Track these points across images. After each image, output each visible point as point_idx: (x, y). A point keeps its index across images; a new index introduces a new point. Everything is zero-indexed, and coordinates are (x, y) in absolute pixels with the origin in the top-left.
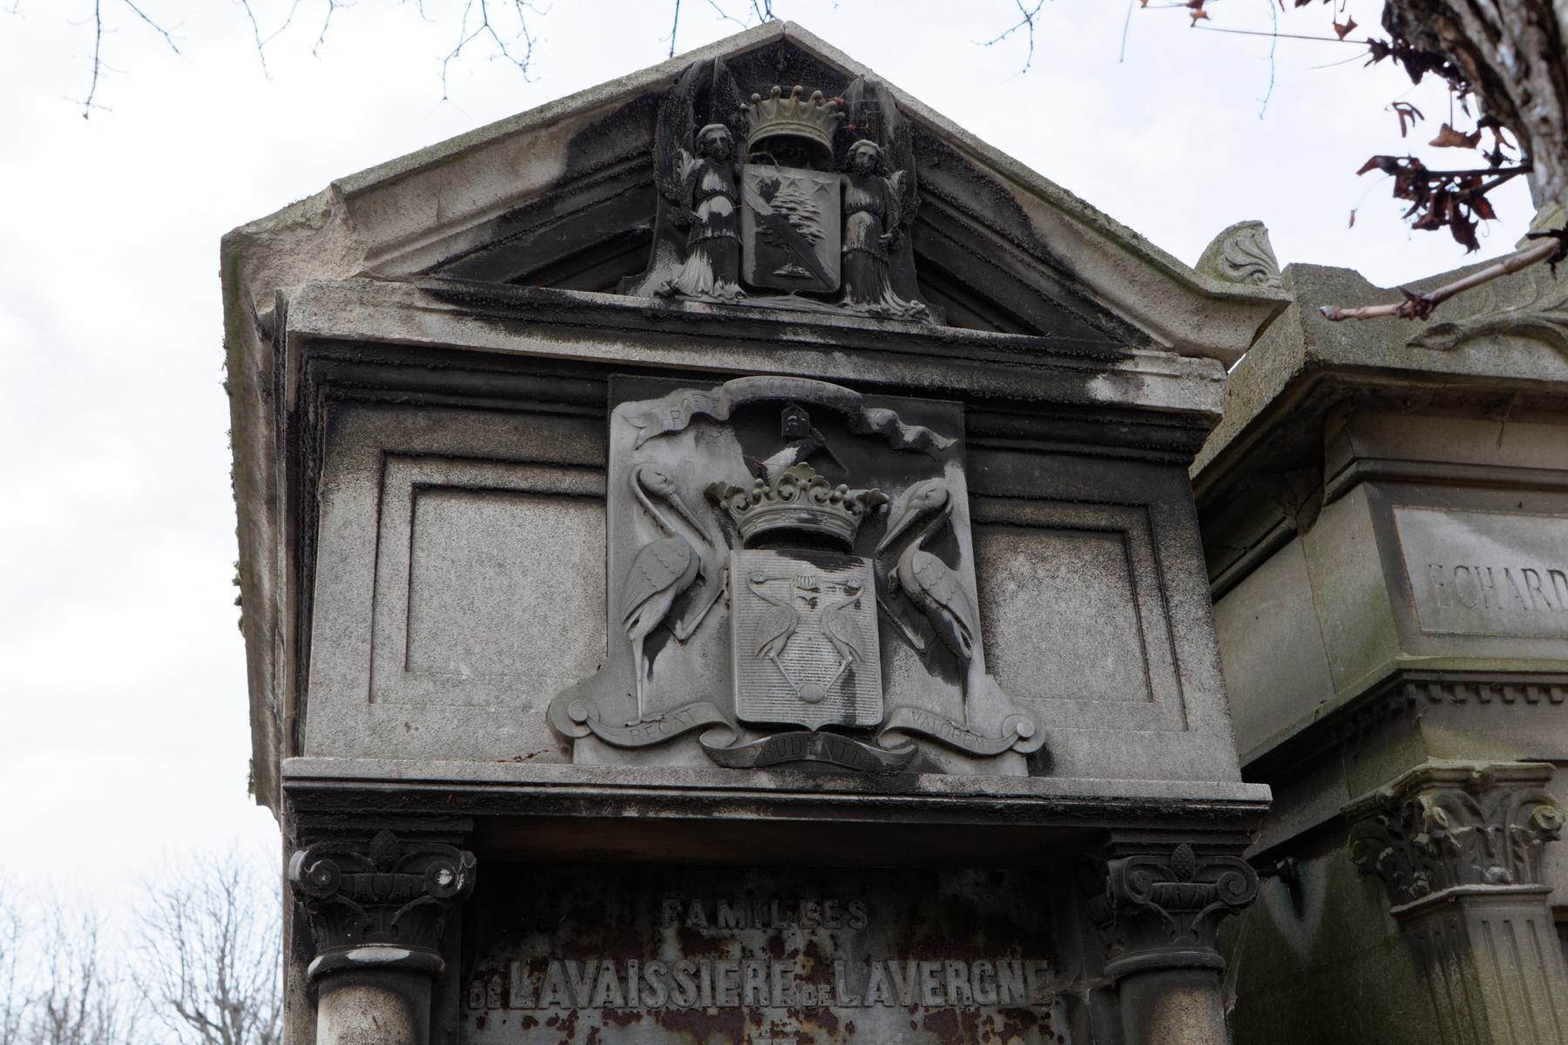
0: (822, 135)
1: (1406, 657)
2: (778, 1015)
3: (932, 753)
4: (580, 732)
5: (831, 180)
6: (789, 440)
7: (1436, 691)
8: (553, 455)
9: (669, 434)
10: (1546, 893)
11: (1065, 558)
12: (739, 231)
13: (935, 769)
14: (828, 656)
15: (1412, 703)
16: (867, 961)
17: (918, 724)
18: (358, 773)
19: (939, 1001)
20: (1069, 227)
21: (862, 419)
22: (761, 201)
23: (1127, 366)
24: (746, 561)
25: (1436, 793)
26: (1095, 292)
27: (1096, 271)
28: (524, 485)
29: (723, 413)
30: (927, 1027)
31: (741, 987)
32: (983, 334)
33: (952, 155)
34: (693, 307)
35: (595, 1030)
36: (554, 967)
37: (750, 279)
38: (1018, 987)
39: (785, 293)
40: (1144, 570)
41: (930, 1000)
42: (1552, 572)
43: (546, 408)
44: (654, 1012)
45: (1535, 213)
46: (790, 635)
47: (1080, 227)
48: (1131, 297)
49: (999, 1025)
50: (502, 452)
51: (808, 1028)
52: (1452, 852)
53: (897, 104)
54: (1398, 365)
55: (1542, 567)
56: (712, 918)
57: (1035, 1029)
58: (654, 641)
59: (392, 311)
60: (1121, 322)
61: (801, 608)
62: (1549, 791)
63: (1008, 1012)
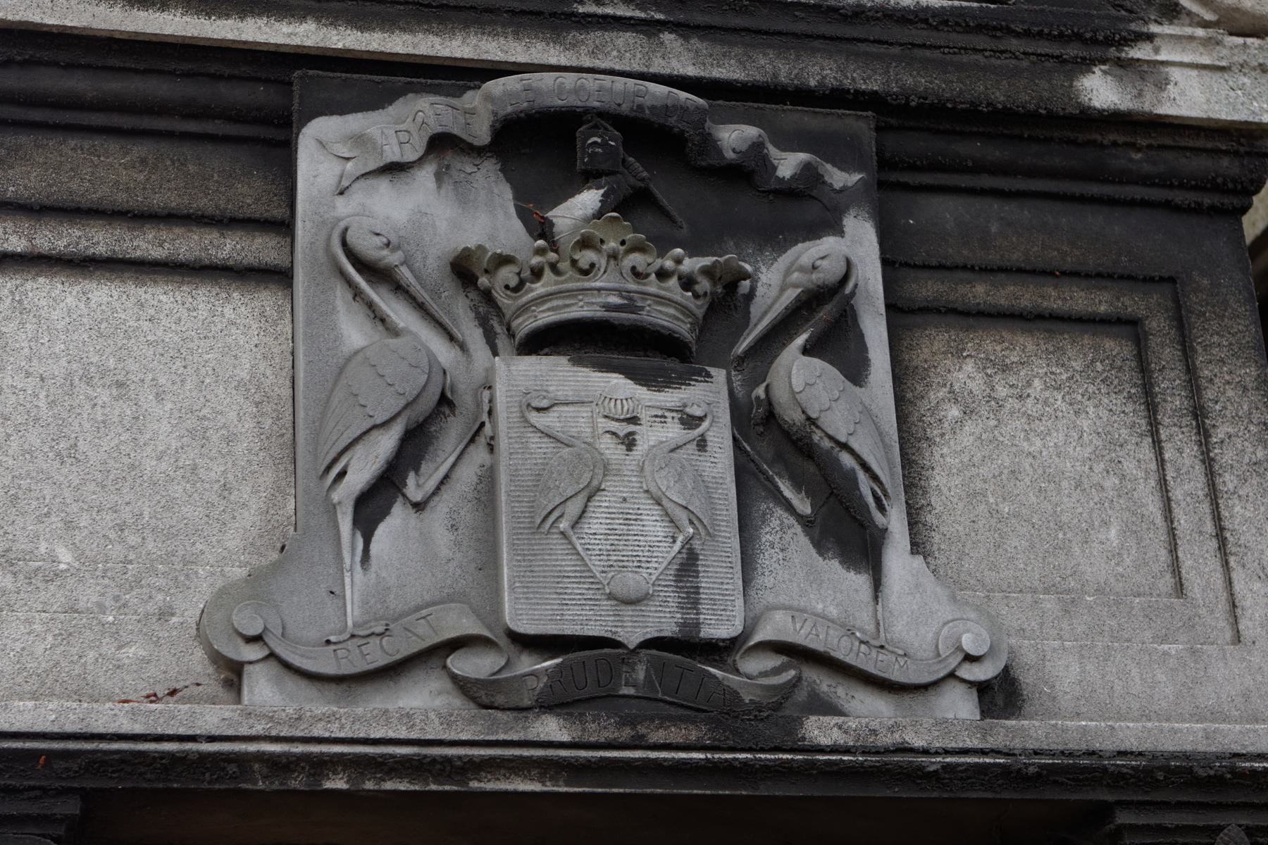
3: (824, 683)
4: (251, 653)
6: (588, 178)
8: (204, 204)
9: (394, 169)
13: (829, 708)
14: (654, 527)
21: (709, 143)
23: (1141, 52)
28: (157, 253)
29: (481, 133)
40: (1170, 383)
43: (192, 126)
46: (593, 493)
61: (610, 449)
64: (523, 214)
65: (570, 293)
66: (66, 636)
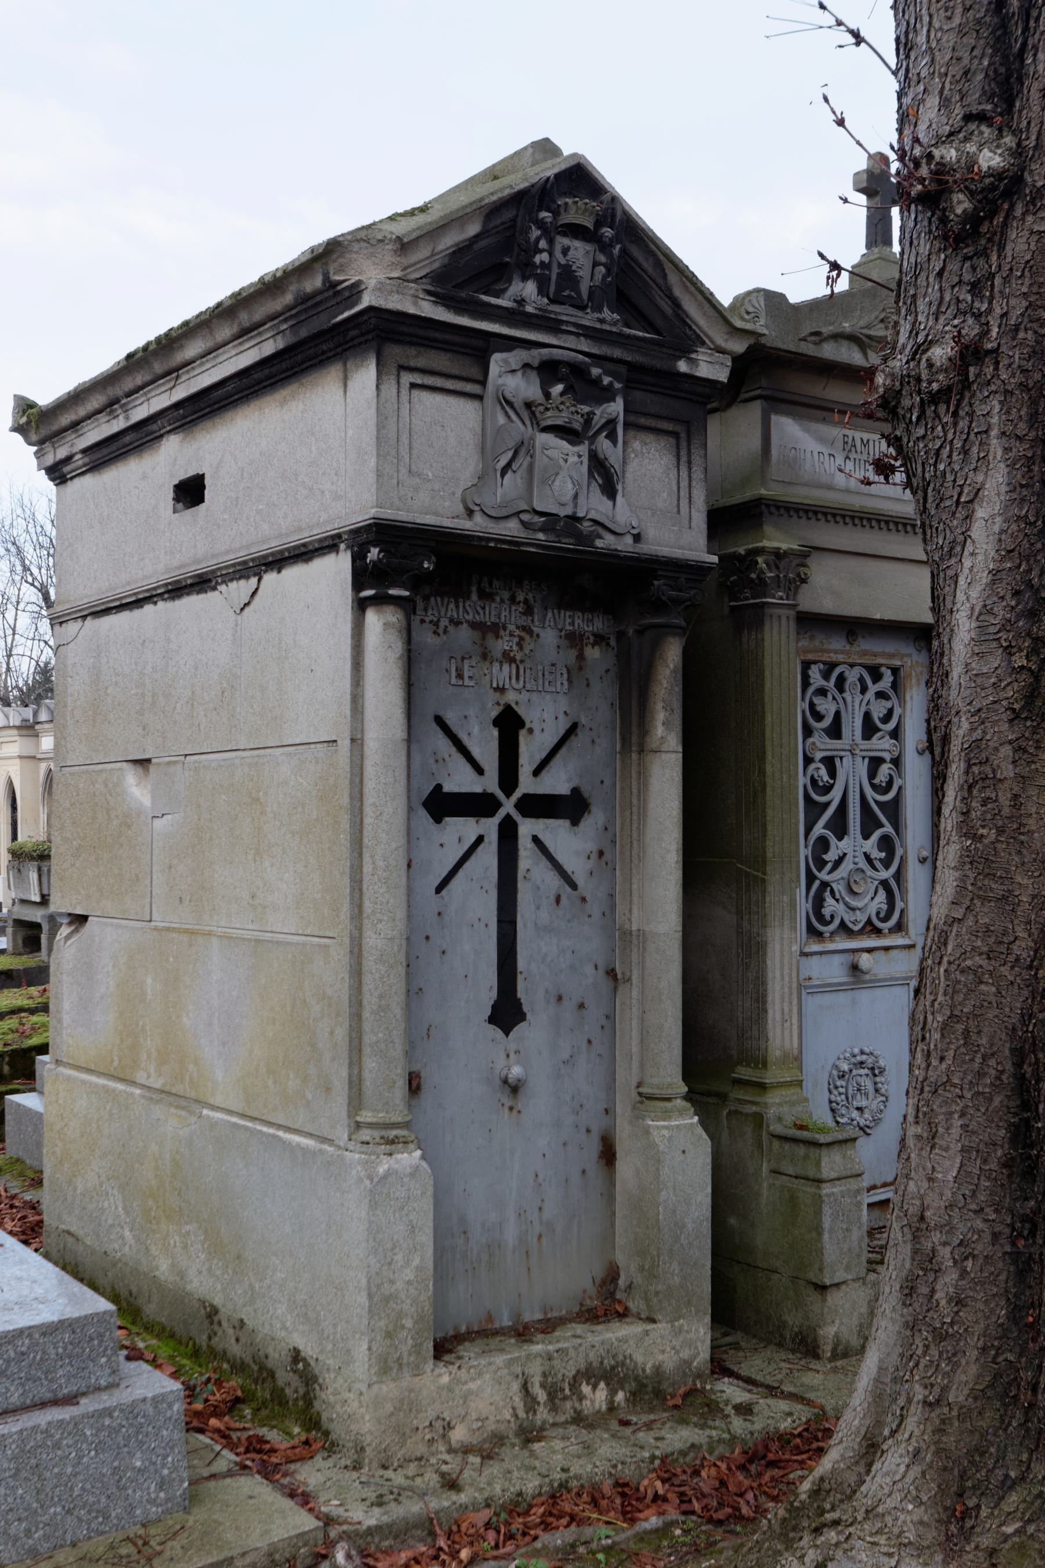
0: (589, 223)
1: (763, 492)
2: (512, 627)
3: (601, 531)
4: (477, 508)
5: (589, 247)
6: (559, 381)
7: (773, 509)
8: (464, 374)
9: (513, 371)
10: (796, 605)
11: (654, 445)
12: (550, 271)
13: (601, 537)
14: (570, 485)
15: (761, 513)
16: (546, 609)
17: (598, 518)
18: (400, 519)
19: (571, 628)
20: (684, 283)
21: (589, 373)
22: (561, 256)
23: (693, 356)
24: (543, 438)
25: (765, 557)
26: (687, 316)
27: (690, 307)
28: (452, 388)
29: (536, 364)
30: (566, 638)
31: (500, 614)
32: (641, 334)
33: (641, 238)
34: (529, 309)
35: (446, 627)
36: (432, 599)
37: (551, 296)
38: (600, 625)
39: (564, 304)
40: (683, 453)
41: (568, 627)
42: (830, 455)
43: (463, 350)
44: (467, 622)
45: (865, 251)
46: (557, 474)
47: (689, 284)
48: (702, 321)
49: (591, 641)
50: (444, 370)
51: (523, 634)
52: (766, 584)
53: (623, 208)
54: (794, 350)
55: (826, 452)
56: (491, 585)
57: (604, 644)
58: (504, 471)
59: (409, 298)
60: (695, 332)
61: (561, 462)
62: (808, 561)
63: (595, 635)
64: (542, 388)
65: (556, 417)
66: (433, 498)
